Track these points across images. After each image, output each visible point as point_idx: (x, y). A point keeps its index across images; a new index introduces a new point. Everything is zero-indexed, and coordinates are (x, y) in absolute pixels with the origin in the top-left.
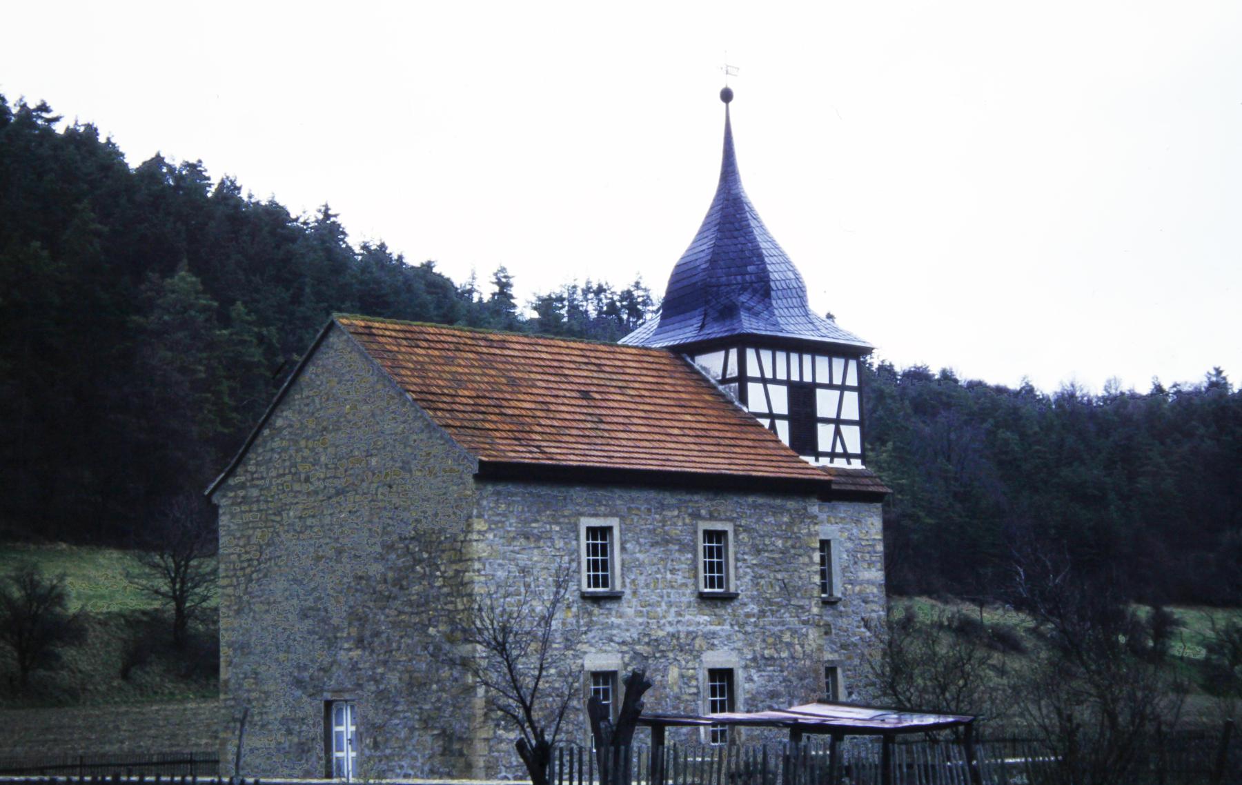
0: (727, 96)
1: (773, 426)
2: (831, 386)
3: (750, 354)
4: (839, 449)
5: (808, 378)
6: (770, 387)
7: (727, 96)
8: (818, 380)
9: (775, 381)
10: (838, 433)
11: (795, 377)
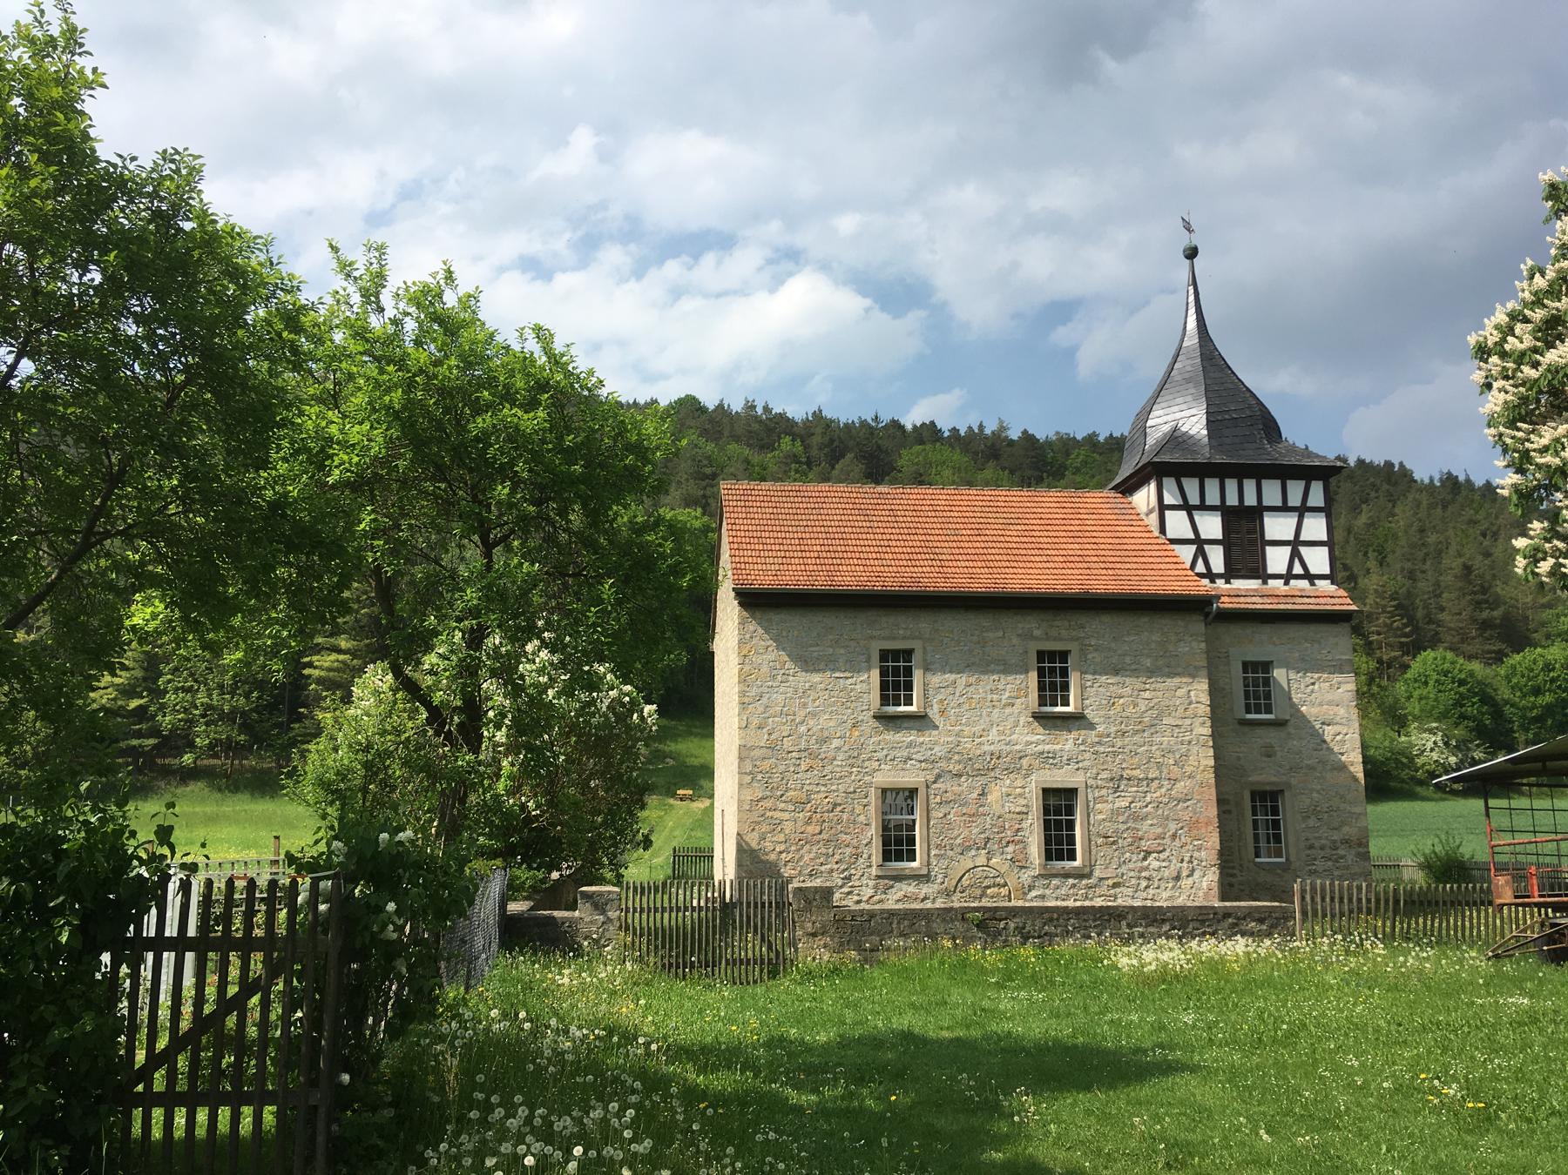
1: (1201, 553)
2: (1285, 508)
4: (1298, 569)
5: (1250, 500)
8: (1265, 503)
9: (1203, 507)
10: (1295, 554)
11: (1232, 500)
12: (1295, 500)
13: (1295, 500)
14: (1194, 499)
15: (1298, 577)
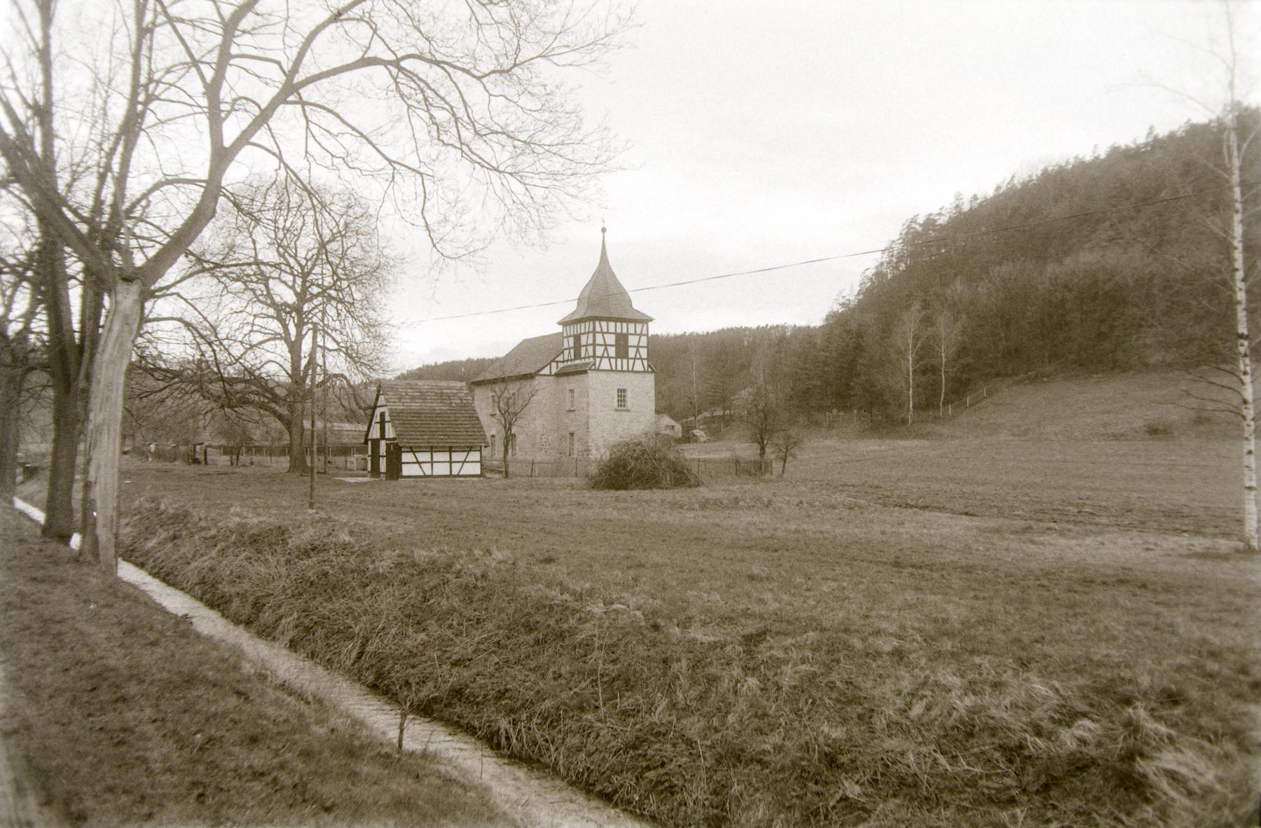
0: (604, 230)
1: (606, 349)
2: (635, 334)
3: (597, 323)
5: (625, 331)
6: (606, 336)
7: (604, 230)
8: (399, 56)
9: (608, 332)
10: (638, 350)
11: (619, 331)
12: (638, 332)
13: (638, 332)
14: (605, 330)
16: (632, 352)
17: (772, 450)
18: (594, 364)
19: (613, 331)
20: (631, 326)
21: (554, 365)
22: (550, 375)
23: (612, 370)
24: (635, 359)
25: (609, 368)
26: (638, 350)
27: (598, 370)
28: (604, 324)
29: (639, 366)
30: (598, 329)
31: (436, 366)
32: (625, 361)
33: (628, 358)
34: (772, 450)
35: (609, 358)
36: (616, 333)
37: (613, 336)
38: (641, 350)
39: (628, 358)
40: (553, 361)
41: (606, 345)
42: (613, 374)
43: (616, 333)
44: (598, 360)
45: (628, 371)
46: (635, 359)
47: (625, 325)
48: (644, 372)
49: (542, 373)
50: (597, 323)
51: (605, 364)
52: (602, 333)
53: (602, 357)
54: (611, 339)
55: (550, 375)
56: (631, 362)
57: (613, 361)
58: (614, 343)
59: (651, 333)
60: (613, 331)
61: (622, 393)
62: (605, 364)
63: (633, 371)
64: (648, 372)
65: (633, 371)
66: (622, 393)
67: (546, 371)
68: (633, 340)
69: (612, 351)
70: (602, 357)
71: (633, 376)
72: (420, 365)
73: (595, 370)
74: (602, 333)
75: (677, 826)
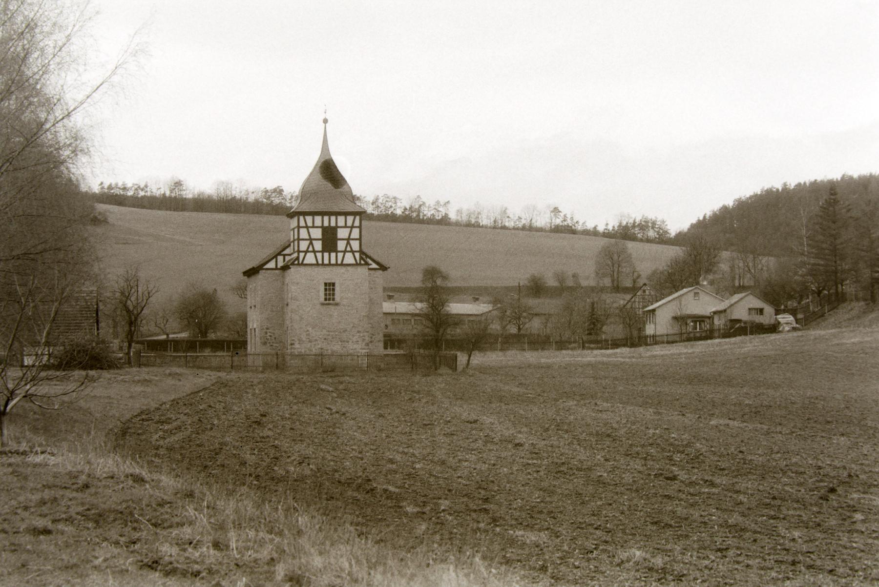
0: (325, 121)
1: (311, 243)
2: (346, 227)
3: (301, 218)
4: (349, 249)
5: (333, 224)
6: (311, 230)
7: (325, 121)
9: (313, 227)
10: (348, 243)
11: (326, 224)
12: (349, 223)
13: (349, 223)
14: (310, 224)
15: (348, 252)
16: (341, 245)
17: (771, 264)
18: (298, 258)
19: (320, 225)
20: (341, 220)
21: (280, 258)
22: (276, 269)
23: (317, 264)
24: (345, 252)
25: (314, 262)
26: (348, 243)
27: (302, 264)
28: (309, 219)
29: (349, 259)
30: (302, 224)
31: (785, 189)
32: (333, 255)
33: (337, 252)
34: (771, 264)
35: (314, 252)
36: (322, 227)
37: (320, 230)
38: (352, 242)
39: (337, 252)
40: (279, 254)
41: (311, 240)
42: (316, 269)
43: (322, 227)
44: (302, 255)
45: (337, 264)
46: (345, 252)
47: (333, 218)
48: (357, 264)
49: (267, 266)
50: (301, 218)
51: (310, 259)
52: (307, 227)
53: (306, 252)
54: (317, 233)
55: (276, 269)
56: (340, 255)
57: (319, 255)
58: (320, 236)
59: (338, 229)
60: (320, 225)
61: (330, 287)
62: (310, 259)
63: (342, 264)
64: (360, 264)
65: (342, 264)
66: (330, 287)
67: (272, 265)
68: (342, 233)
69: (318, 246)
70: (306, 252)
71: (342, 270)
72: (752, 194)
73: (298, 264)
74: (307, 227)
75: (600, 586)
